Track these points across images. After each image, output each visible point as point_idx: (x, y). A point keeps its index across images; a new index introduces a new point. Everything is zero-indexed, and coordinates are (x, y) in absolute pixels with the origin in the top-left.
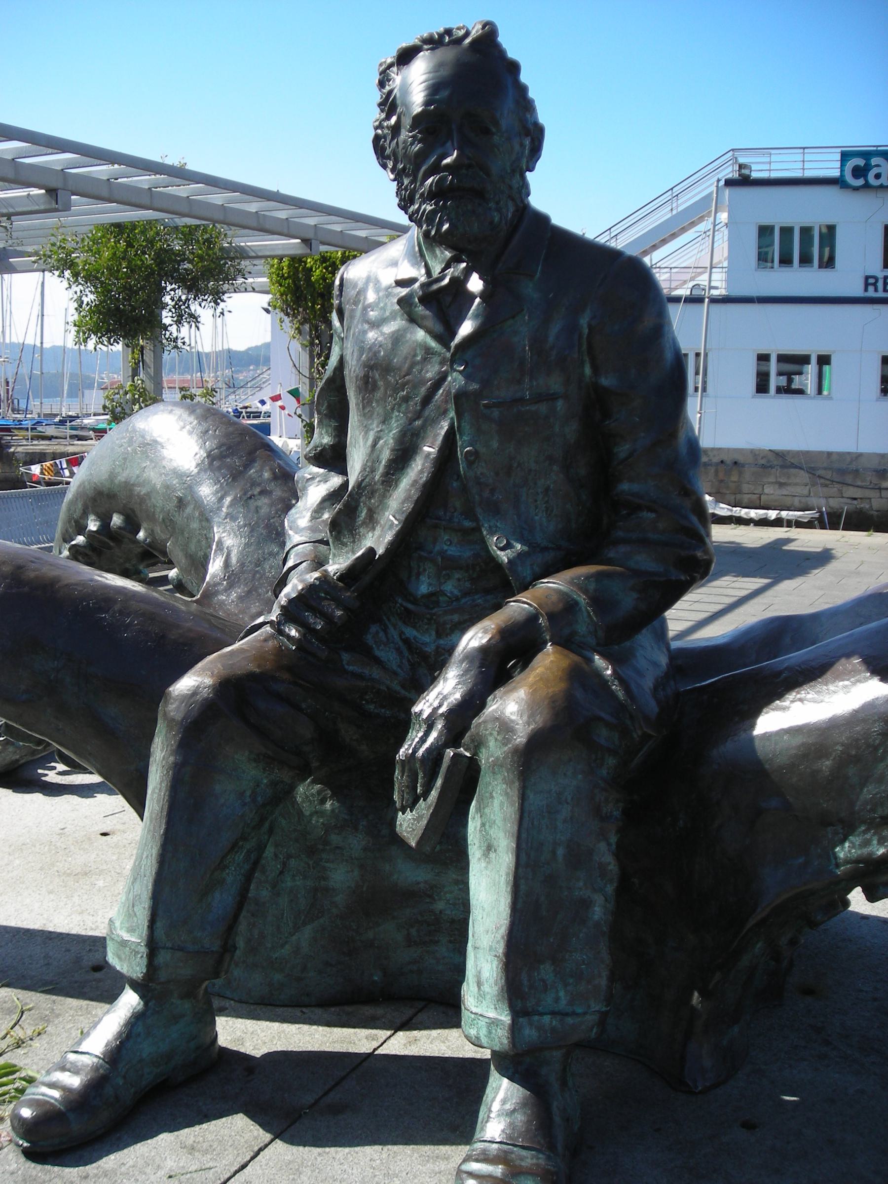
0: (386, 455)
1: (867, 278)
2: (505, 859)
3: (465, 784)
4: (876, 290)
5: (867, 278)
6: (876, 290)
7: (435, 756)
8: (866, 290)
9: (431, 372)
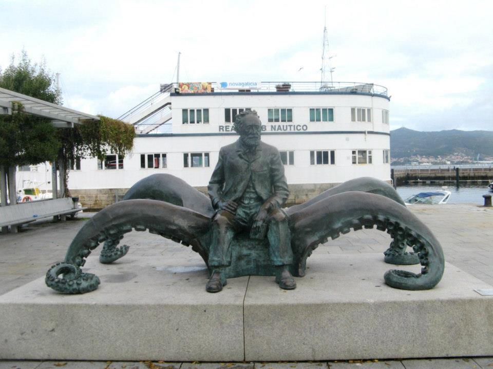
1: (220, 126)
4: (223, 131)
5: (220, 126)
6: (223, 131)
8: (220, 131)
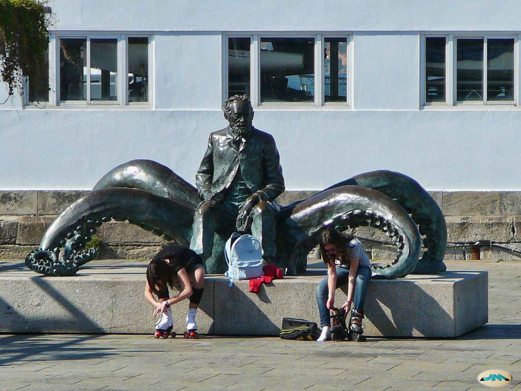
0: (226, 171)
2: (260, 228)
3: (251, 221)
7: (245, 217)
9: (235, 155)
